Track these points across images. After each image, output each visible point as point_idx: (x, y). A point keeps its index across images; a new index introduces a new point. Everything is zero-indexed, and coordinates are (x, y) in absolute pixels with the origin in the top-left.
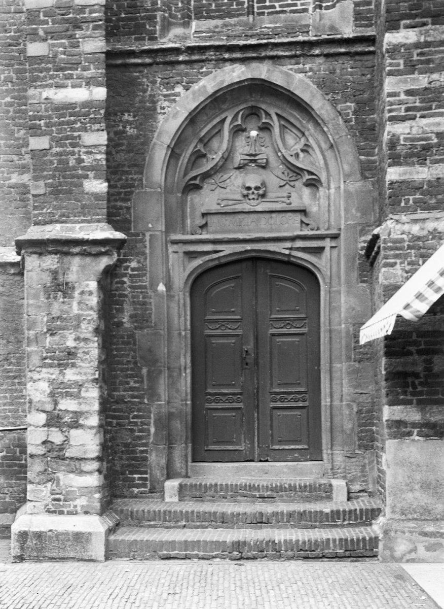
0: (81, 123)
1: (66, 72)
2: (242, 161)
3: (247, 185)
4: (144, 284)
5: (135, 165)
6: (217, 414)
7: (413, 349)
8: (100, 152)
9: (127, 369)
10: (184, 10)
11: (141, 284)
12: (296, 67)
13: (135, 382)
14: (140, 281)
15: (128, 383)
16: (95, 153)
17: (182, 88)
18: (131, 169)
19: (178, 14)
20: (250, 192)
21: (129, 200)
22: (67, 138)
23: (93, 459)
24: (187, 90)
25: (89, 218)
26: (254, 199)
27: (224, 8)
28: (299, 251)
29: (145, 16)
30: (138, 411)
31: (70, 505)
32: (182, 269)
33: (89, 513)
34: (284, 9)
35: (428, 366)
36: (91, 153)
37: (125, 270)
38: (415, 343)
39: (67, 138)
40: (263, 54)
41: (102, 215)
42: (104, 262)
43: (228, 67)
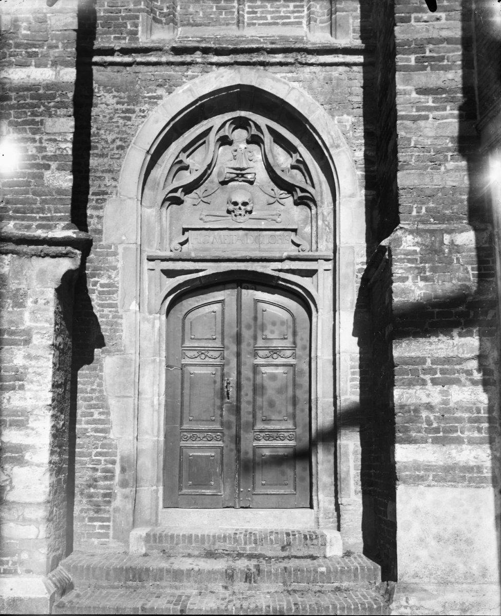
0: (44, 106)
1: (29, 50)
2: (228, 175)
3: (233, 200)
4: (115, 302)
5: (110, 171)
6: (194, 454)
7: (427, 377)
8: (66, 141)
9: (92, 399)
10: (169, 15)
11: (111, 302)
12: (290, 75)
13: (100, 413)
14: (110, 298)
15: (92, 415)
16: (59, 141)
17: (165, 91)
18: (104, 175)
19: (163, 19)
20: (237, 207)
21: (101, 208)
23: (39, 504)
24: (170, 93)
25: (49, 215)
26: (240, 215)
27: (212, 16)
28: (288, 273)
29: (126, 15)
30: (103, 446)
31: (8, 562)
32: (158, 289)
33: (31, 571)
34: (276, 21)
35: (445, 398)
36: (55, 140)
37: (93, 286)
38: (431, 371)
40: (254, 60)
41: (65, 212)
42: (66, 265)
43: (216, 71)
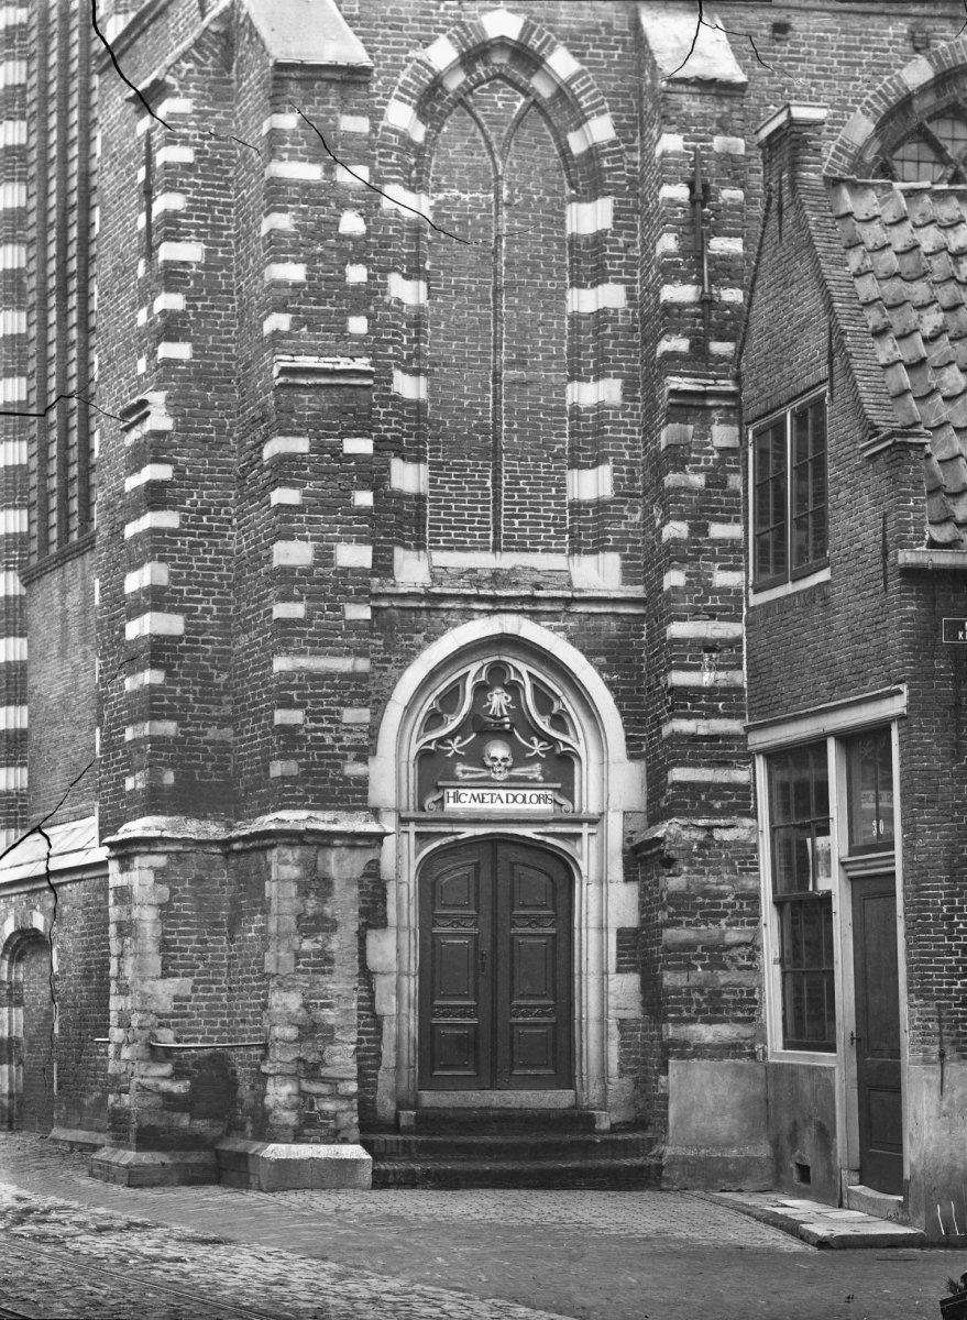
12: (556, 624)
22: (324, 712)
39: (324, 712)
